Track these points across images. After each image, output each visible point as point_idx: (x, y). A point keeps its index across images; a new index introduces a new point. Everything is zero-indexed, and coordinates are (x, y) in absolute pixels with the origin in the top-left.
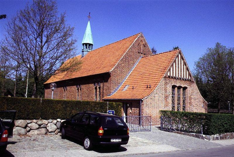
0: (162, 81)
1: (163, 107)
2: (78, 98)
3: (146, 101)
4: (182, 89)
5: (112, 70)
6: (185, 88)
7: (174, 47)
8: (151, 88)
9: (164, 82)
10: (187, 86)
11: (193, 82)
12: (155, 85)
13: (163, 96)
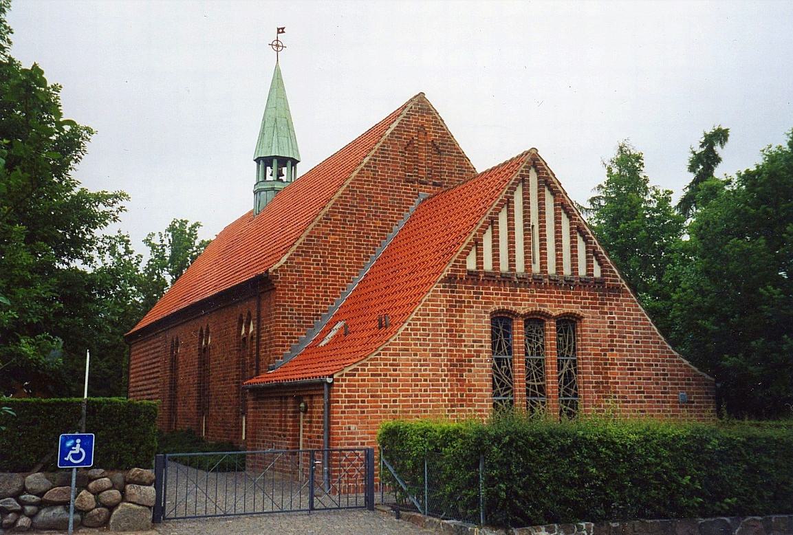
0: (434, 298)
2: (143, 326)
6: (568, 323)
9: (442, 301)
10: (578, 311)
11: (617, 290)
13: (443, 360)
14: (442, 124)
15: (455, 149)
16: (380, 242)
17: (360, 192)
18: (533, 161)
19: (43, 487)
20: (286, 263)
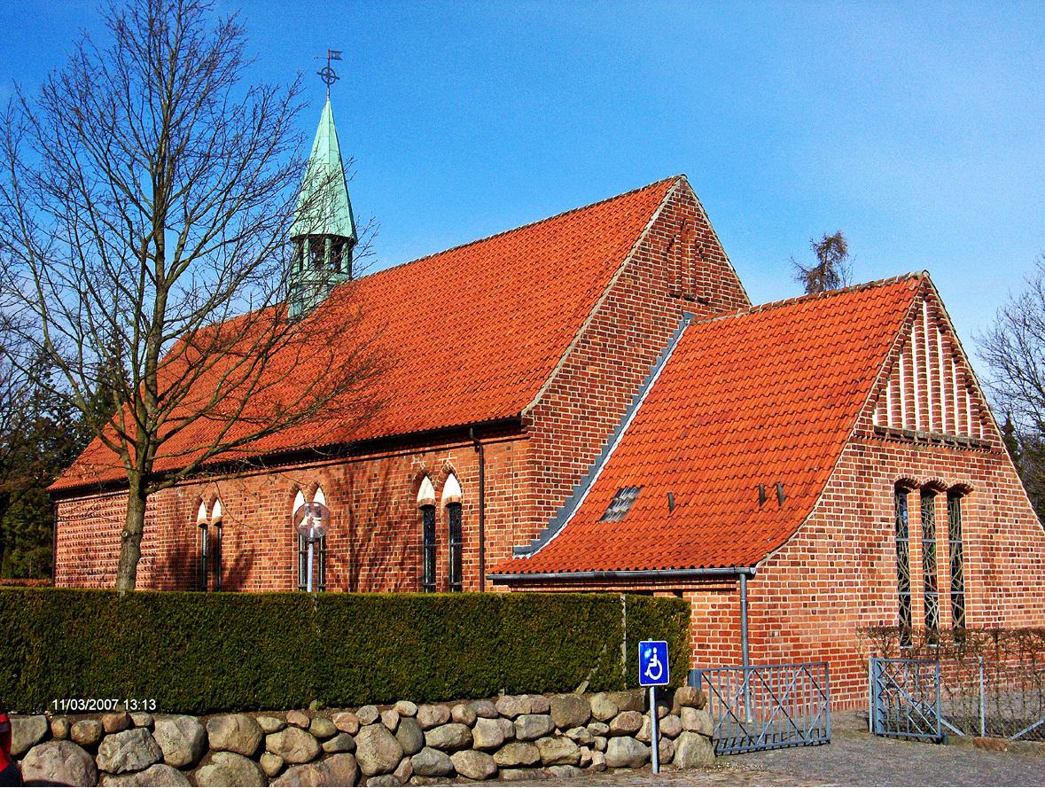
1: (854, 604)
3: (770, 578)
4: (941, 497)
5: (535, 402)
6: (957, 492)
7: (819, 240)
8: (786, 504)
10: (968, 481)
12: (810, 490)
14: (705, 219)
15: (719, 254)
16: (643, 377)
17: (621, 306)
18: (926, 290)
19: (608, 716)
20: (541, 402)
